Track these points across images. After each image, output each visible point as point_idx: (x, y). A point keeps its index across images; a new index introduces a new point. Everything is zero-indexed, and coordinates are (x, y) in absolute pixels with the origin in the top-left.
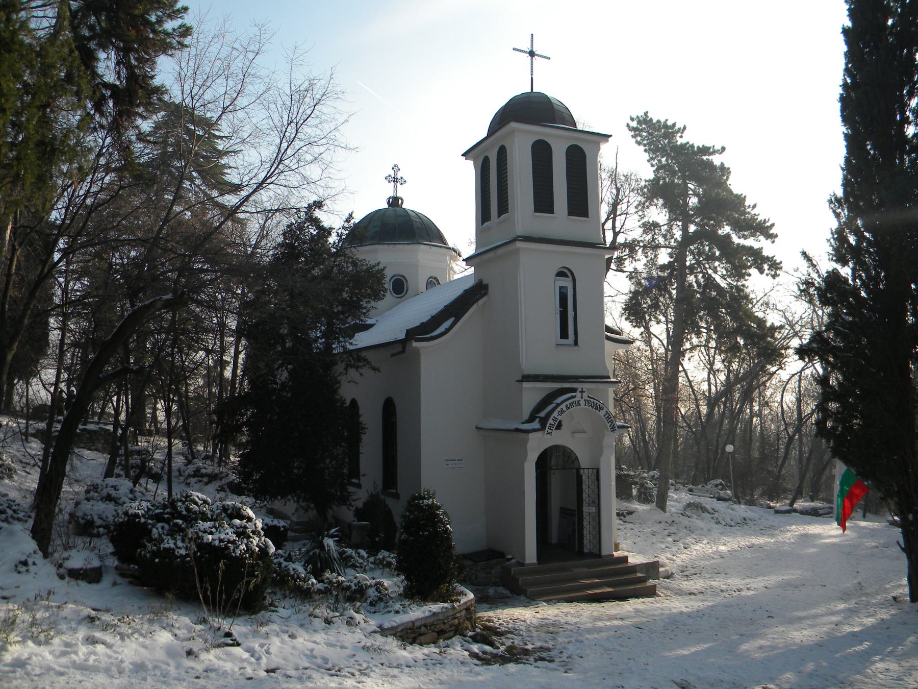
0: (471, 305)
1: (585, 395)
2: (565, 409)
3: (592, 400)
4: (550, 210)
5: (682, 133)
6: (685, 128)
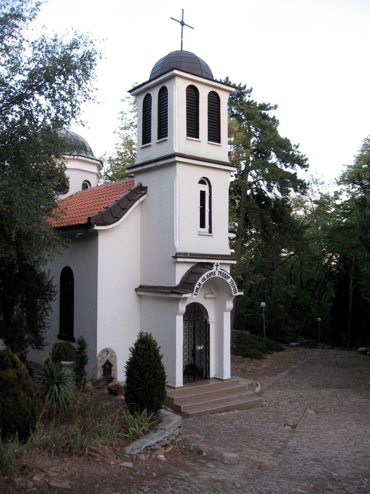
0: (135, 201)
1: (219, 267)
2: (206, 278)
3: (223, 272)
4: (197, 136)
5: (250, 93)
6: (251, 90)
